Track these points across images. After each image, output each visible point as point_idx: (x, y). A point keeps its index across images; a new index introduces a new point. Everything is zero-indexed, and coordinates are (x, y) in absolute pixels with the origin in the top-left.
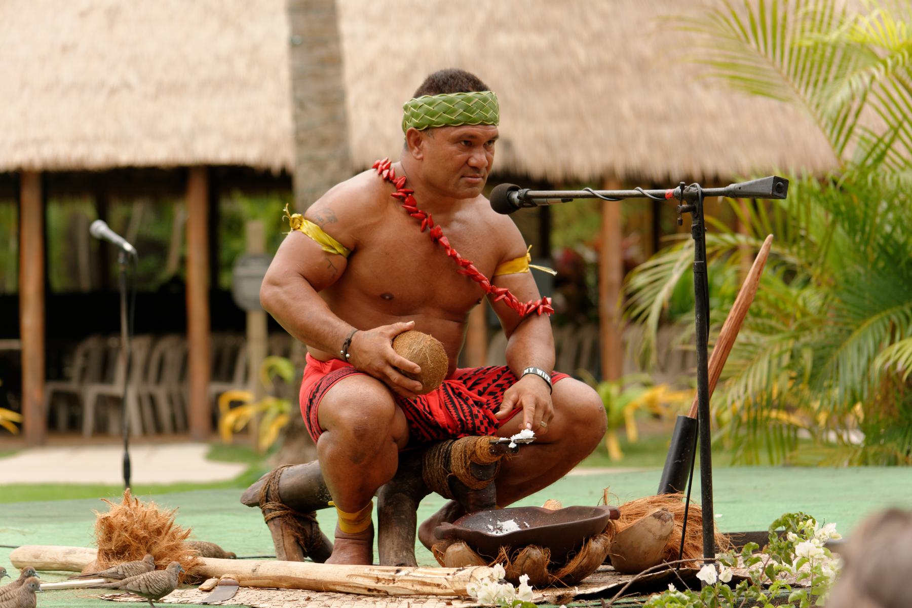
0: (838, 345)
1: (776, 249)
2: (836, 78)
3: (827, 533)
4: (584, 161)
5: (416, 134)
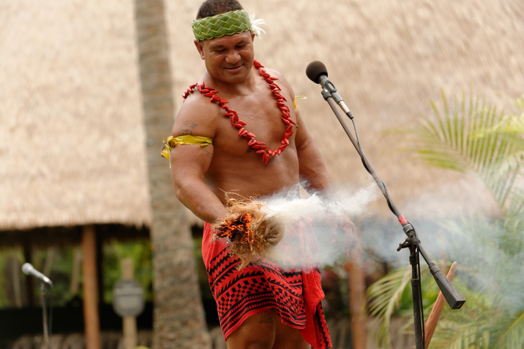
2: (497, 159)
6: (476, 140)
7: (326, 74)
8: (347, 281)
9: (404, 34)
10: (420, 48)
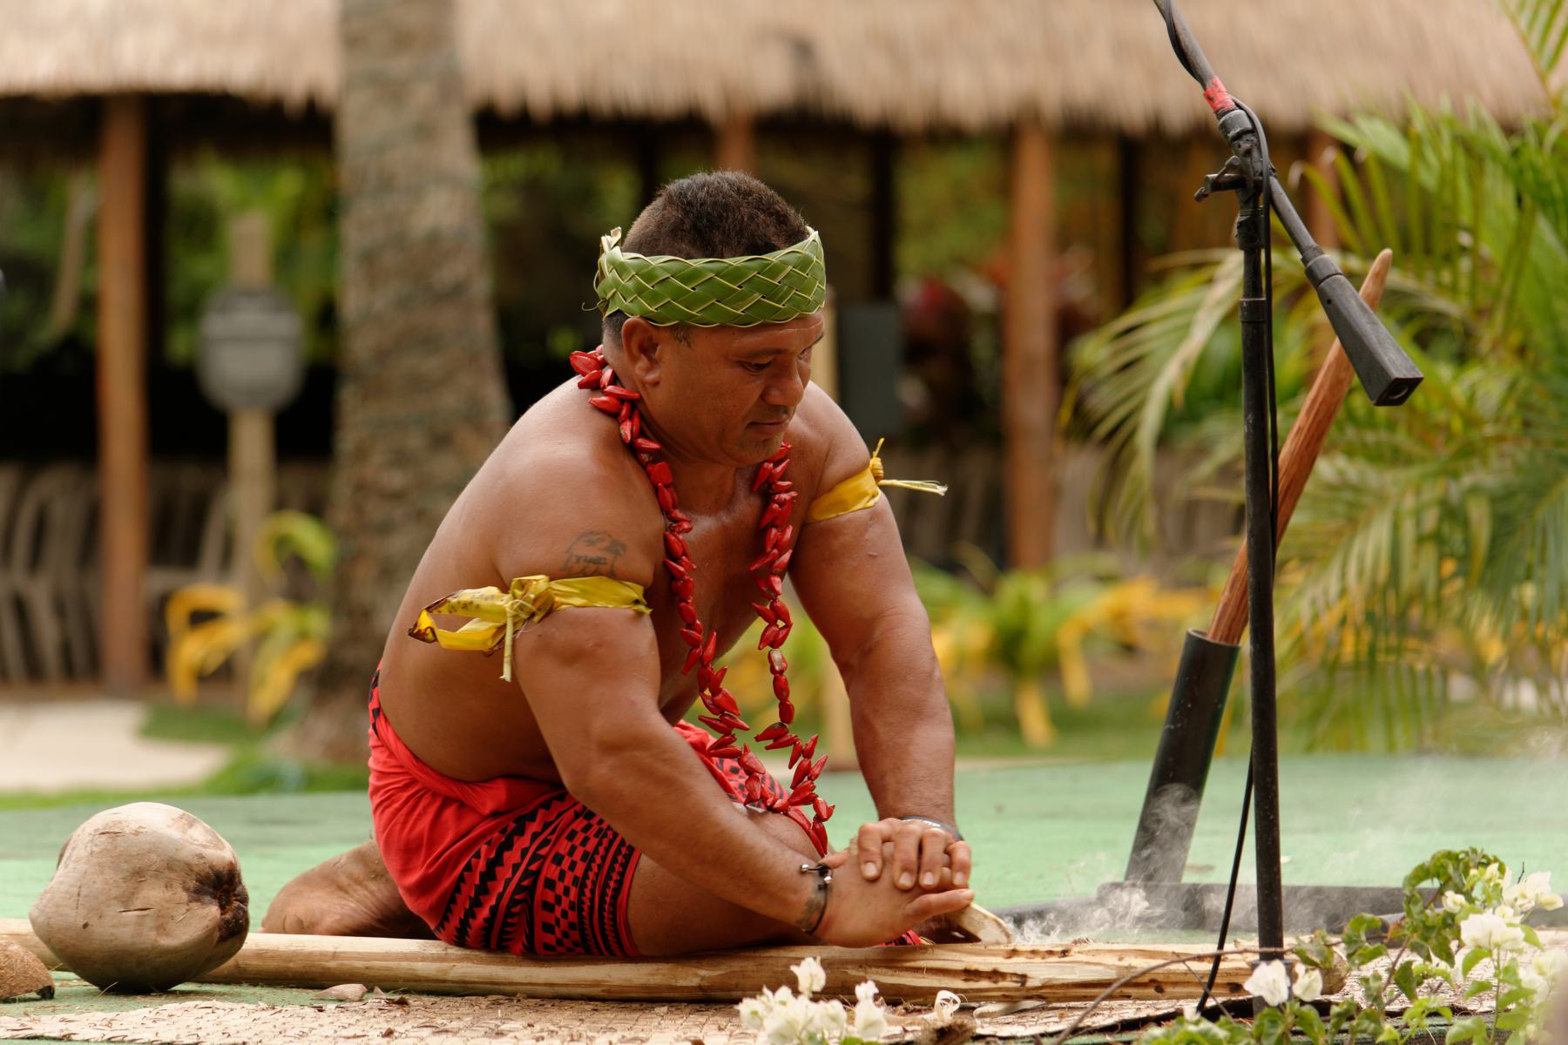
0: (1539, 492)
1: (1395, 278)
3: (1531, 895)
4: (972, 88)
8: (998, 321)
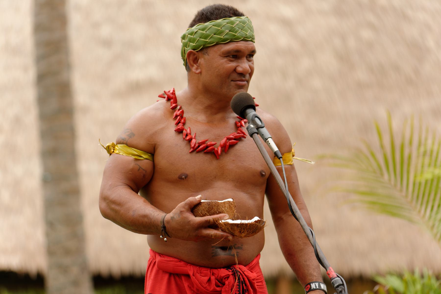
5: (194, 54)
6: (423, 182)
7: (253, 107)
9: (344, 58)
10: (361, 74)
